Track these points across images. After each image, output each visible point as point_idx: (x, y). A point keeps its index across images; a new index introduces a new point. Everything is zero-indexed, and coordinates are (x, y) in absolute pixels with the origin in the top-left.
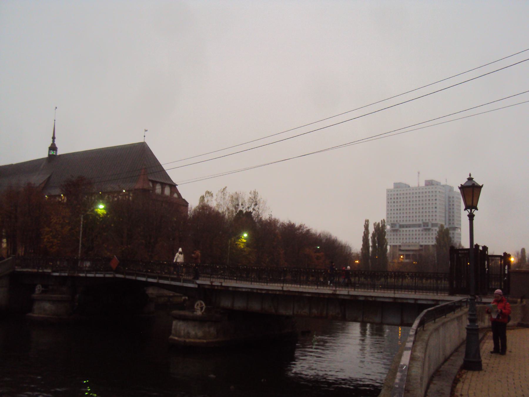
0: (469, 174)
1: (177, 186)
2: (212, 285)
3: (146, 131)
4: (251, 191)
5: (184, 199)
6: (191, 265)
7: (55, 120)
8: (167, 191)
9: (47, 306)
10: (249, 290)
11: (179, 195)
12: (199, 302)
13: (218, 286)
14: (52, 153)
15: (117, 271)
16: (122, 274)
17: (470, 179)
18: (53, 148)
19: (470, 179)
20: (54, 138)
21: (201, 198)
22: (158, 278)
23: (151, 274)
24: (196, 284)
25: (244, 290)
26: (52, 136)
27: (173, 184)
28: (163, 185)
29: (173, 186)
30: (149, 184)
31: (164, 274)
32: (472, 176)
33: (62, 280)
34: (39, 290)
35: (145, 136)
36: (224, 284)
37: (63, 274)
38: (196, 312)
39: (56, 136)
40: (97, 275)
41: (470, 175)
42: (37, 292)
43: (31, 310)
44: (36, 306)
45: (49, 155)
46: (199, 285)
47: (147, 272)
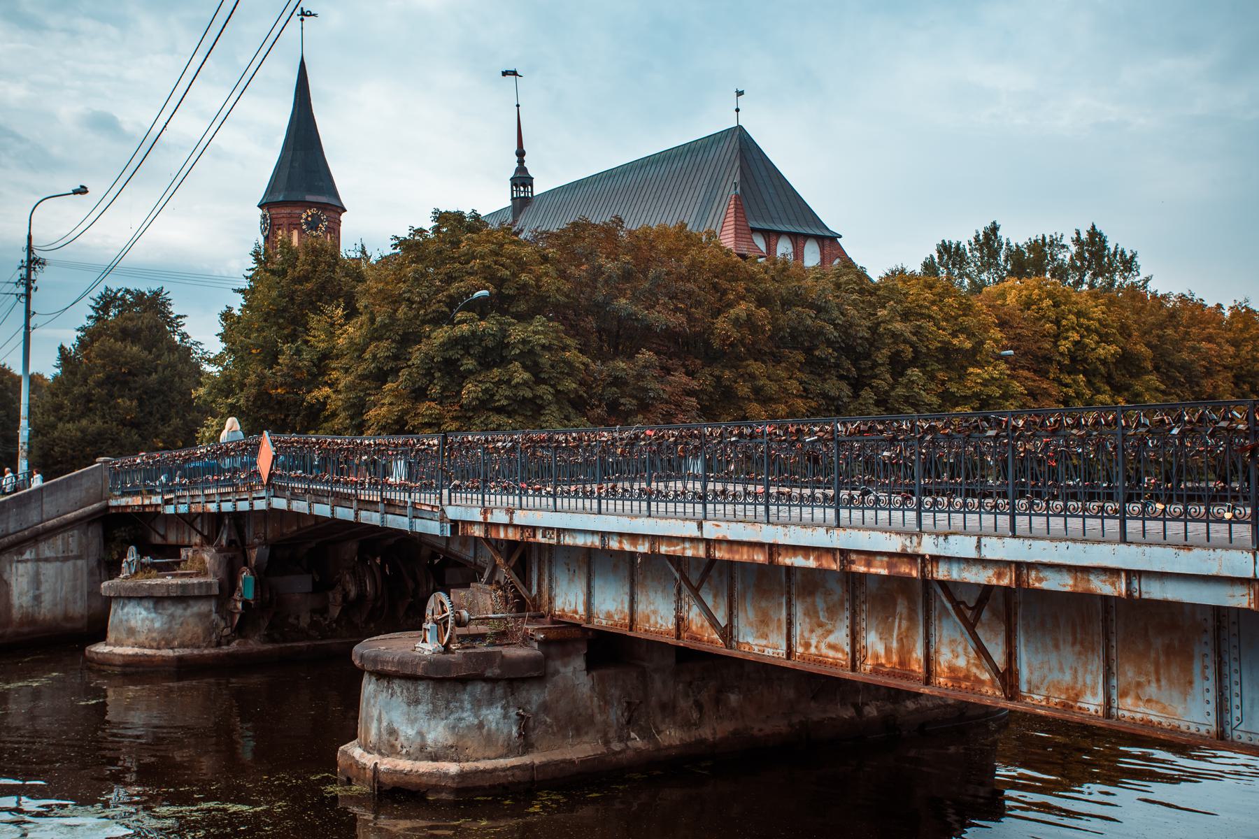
3: (740, 93)
4: (1078, 233)
7: (518, 106)
8: (812, 256)
18: (522, 179)
20: (521, 153)
26: (515, 148)
27: (828, 234)
28: (798, 239)
29: (829, 241)
35: (737, 110)
45: (513, 199)
46: (455, 524)
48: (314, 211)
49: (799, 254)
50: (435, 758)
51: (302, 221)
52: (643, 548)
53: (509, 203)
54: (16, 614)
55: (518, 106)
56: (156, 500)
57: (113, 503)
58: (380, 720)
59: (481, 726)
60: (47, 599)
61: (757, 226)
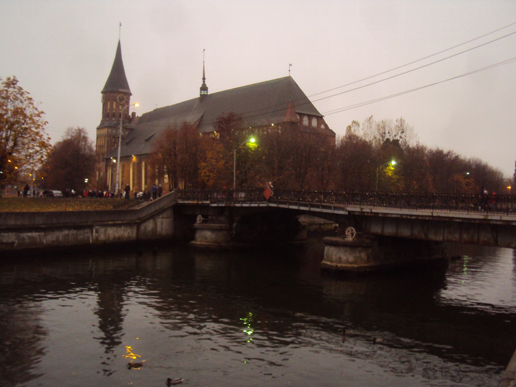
1: (323, 118)
2: (362, 212)
3: (290, 65)
8: (314, 123)
10: (399, 216)
12: (349, 228)
13: (367, 213)
14: (204, 93)
15: (270, 200)
18: (204, 88)
20: (204, 79)
22: (309, 206)
24: (347, 210)
25: (393, 216)
26: (202, 77)
27: (320, 115)
28: (310, 117)
29: (320, 118)
33: (220, 211)
34: (200, 220)
35: (289, 71)
36: (373, 211)
39: (206, 77)
42: (198, 222)
43: (193, 238)
44: (198, 235)
45: (201, 95)
46: (349, 212)
47: (299, 200)
48: (122, 95)
50: (351, 263)
51: (118, 98)
52: (413, 218)
54: (158, 233)
55: (204, 62)
56: (208, 202)
58: (336, 255)
59: (360, 257)
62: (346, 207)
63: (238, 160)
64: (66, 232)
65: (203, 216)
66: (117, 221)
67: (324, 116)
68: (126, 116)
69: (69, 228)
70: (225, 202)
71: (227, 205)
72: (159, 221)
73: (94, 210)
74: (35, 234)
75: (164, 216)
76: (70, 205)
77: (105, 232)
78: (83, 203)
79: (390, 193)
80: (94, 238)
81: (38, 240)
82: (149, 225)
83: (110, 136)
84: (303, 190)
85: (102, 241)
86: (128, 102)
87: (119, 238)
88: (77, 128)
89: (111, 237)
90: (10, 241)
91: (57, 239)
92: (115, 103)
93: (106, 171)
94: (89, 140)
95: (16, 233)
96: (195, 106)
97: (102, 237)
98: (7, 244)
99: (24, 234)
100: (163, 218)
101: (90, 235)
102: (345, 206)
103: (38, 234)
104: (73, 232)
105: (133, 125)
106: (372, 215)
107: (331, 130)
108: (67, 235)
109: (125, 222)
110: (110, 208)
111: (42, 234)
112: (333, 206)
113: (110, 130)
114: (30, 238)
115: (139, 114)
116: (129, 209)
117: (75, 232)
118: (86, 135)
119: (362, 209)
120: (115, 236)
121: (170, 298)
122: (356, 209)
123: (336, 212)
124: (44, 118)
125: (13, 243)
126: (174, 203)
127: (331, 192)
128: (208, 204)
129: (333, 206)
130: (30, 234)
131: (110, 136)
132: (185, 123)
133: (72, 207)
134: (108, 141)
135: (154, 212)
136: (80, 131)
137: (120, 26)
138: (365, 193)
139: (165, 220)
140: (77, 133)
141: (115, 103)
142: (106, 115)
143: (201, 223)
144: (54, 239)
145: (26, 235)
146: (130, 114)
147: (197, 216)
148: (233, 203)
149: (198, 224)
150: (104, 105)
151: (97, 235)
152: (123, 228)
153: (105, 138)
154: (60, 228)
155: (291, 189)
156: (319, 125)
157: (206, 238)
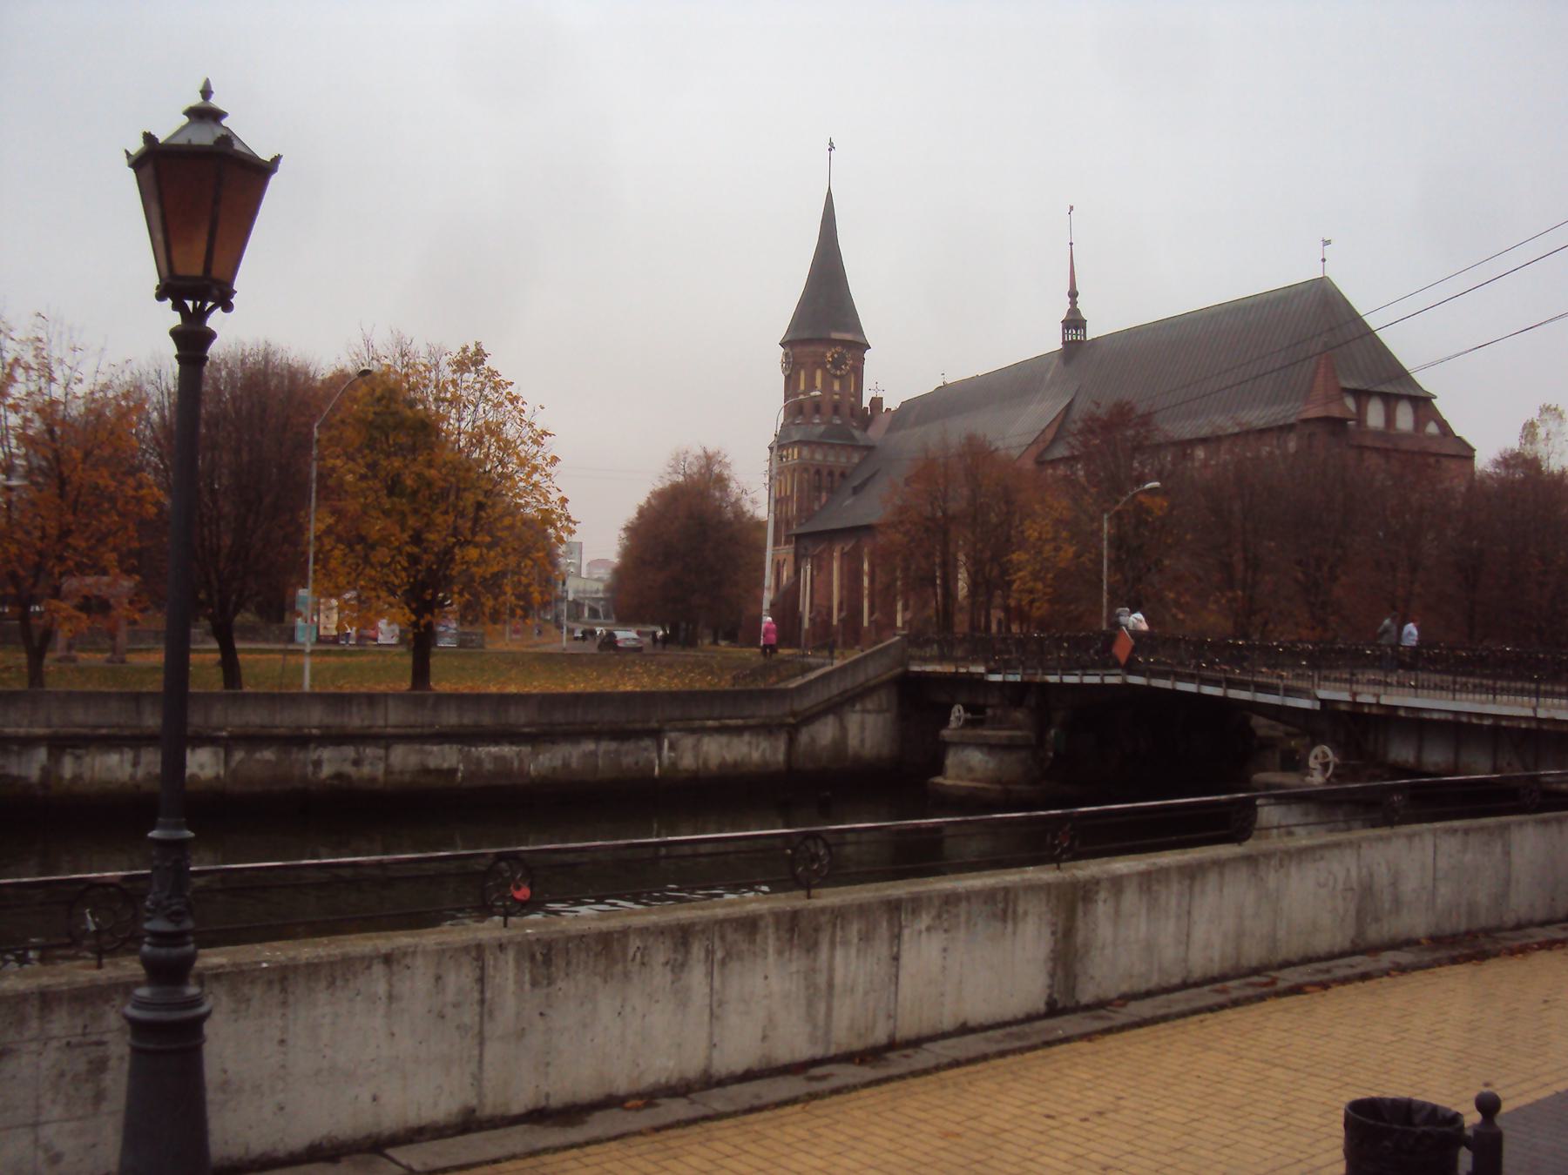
0: (200, 86)
1: (1433, 400)
2: (1354, 704)
3: (1326, 243)
5: (1459, 437)
6: (1301, 647)
8: (1405, 419)
9: (976, 758)
10: (1450, 717)
11: (1443, 426)
12: (1317, 750)
13: (1370, 705)
14: (1073, 335)
15: (1130, 667)
16: (1141, 674)
17: (204, 114)
18: (1074, 322)
19: (204, 114)
20: (1073, 294)
21: (1524, 429)
22: (1224, 685)
23: (1209, 673)
24: (1317, 698)
25: (1436, 716)
26: (1068, 289)
27: (1423, 395)
28: (1390, 400)
29: (1422, 403)
30: (1344, 405)
31: (1239, 674)
32: (216, 102)
33: (1016, 694)
34: (959, 718)
35: (1324, 260)
36: (1384, 700)
37: (1011, 678)
38: (1312, 776)
40: (1088, 680)
41: (206, 93)
42: (953, 723)
43: (939, 769)
44: (951, 760)
45: (1064, 343)
46: (1323, 701)
47: (1198, 666)
48: (839, 349)
49: (1390, 419)
52: (1487, 722)
53: (1061, 347)
54: (851, 751)
55: (1071, 244)
57: (915, 668)
60: (868, 744)
61: (1348, 386)
62: (1316, 687)
63: (1118, 542)
64: (589, 746)
65: (966, 710)
66: (730, 718)
67: (1435, 397)
68: (852, 409)
69: (597, 735)
70: (1020, 671)
71: (1026, 678)
72: (853, 720)
73: (687, 688)
74: (507, 750)
75: (870, 706)
76: (630, 673)
77: (696, 747)
78: (664, 670)
79: (1424, 651)
80: (666, 762)
81: (516, 764)
82: (824, 732)
83: (806, 470)
84: (1209, 640)
85: (686, 771)
86: (858, 371)
87: (736, 764)
88: (700, 452)
89: (714, 762)
90: (446, 766)
91: (566, 765)
92: (819, 374)
93: (797, 572)
94: (733, 485)
95: (459, 747)
96: (1049, 376)
97: (688, 761)
98: (439, 772)
99: (480, 749)
100: (864, 711)
101: (654, 755)
102: (1313, 685)
103: (515, 748)
104: (607, 746)
105: (875, 434)
106: (1382, 712)
107: (1459, 438)
108: (594, 754)
109: (751, 722)
110: (725, 684)
111: (526, 749)
112: (1281, 686)
113: (806, 452)
114: (497, 759)
115: (891, 403)
116: (777, 687)
117: (613, 746)
118: (726, 473)
119: (1354, 694)
120: (724, 758)
121: (657, 896)
122: (1336, 693)
123: (1292, 702)
124: (551, 446)
125: (452, 772)
126: (899, 670)
127: (1278, 646)
128: (982, 674)
129: (1281, 686)
130: (494, 749)
131: (806, 470)
132: (971, 439)
133: (636, 679)
134: (800, 483)
135: (840, 695)
136: (709, 460)
137: (830, 150)
138: (1364, 650)
139: (870, 719)
140: (701, 467)
141: (819, 374)
142: (796, 410)
143: (962, 727)
144: (558, 763)
145: (487, 752)
146: (866, 403)
147: (950, 707)
148: (1040, 671)
149: (955, 729)
150: (788, 378)
151: (673, 754)
152: (747, 737)
153: (793, 476)
154: (573, 735)
155: (1181, 637)
156: (1419, 423)
157: (970, 770)
